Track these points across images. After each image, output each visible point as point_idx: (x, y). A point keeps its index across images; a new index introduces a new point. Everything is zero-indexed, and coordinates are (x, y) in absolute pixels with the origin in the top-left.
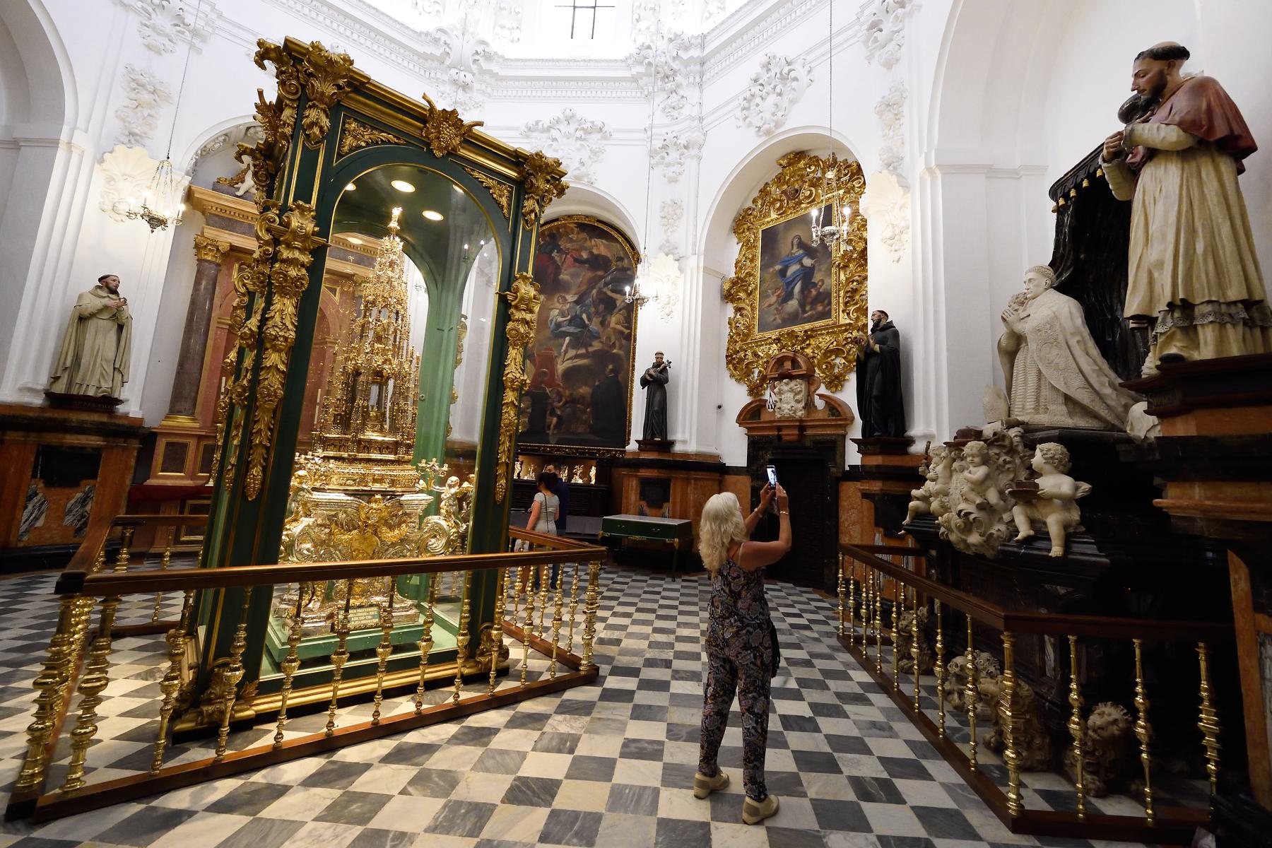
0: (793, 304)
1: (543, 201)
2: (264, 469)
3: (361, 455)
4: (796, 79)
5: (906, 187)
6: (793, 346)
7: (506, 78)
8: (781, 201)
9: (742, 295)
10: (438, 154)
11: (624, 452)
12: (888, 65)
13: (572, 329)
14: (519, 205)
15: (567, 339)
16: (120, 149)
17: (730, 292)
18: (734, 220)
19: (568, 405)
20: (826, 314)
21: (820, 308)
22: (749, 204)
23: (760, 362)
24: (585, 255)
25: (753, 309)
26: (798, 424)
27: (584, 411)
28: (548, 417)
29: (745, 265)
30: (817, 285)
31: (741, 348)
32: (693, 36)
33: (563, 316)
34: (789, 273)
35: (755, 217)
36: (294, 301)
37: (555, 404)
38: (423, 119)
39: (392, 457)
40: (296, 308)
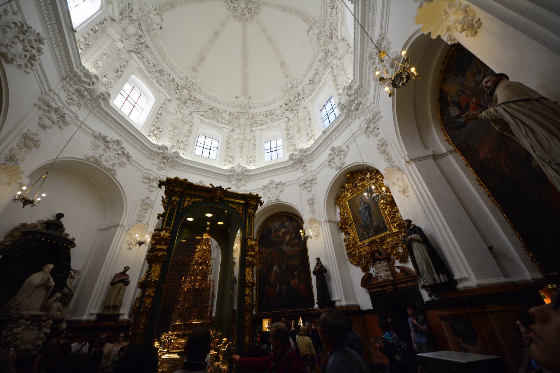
1: (255, 208)
7: (252, 175)
11: (313, 310)
26: (391, 283)
40: (160, 268)
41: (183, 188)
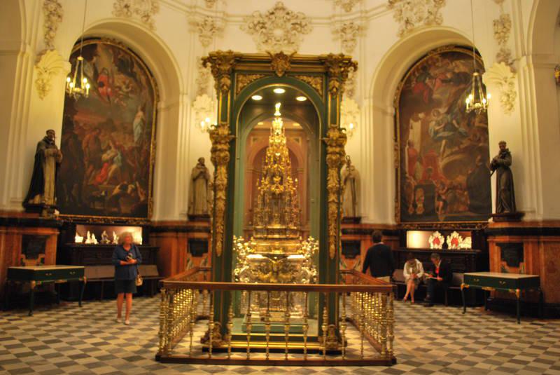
2: (222, 242)
3: (270, 236)
10: (280, 75)
12: (352, 23)
13: (446, 134)
14: (327, 86)
15: (444, 142)
16: (198, 98)
19: (450, 191)
24: (449, 76)
27: (463, 195)
28: (436, 201)
33: (439, 125)
36: (225, 167)
37: (440, 192)
38: (269, 61)
39: (284, 236)
41: (231, 64)
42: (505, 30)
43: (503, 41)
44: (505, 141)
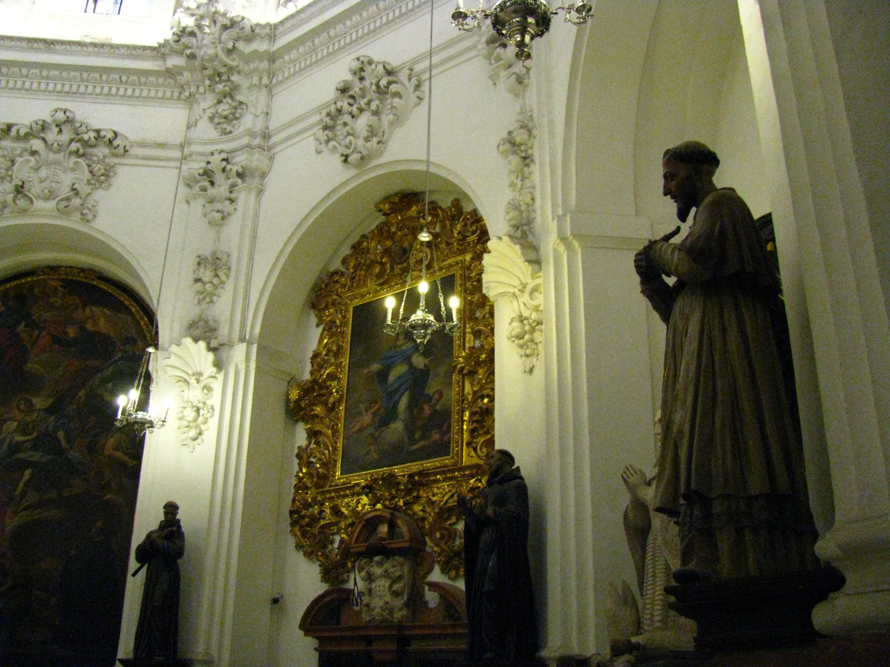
0: (397, 427)
4: (397, 95)
5: (536, 262)
6: (393, 498)
8: (382, 264)
9: (318, 410)
13: (37, 457)
15: (28, 473)
17: (299, 405)
18: (313, 289)
20: (442, 449)
21: (436, 436)
22: (336, 265)
23: (342, 525)
25: (335, 432)
29: (326, 362)
30: (431, 398)
31: (314, 499)
32: (257, 25)
33: (24, 433)
34: (391, 378)
35: (344, 286)
42: (215, 281)
43: (208, 299)
44: (179, 504)
